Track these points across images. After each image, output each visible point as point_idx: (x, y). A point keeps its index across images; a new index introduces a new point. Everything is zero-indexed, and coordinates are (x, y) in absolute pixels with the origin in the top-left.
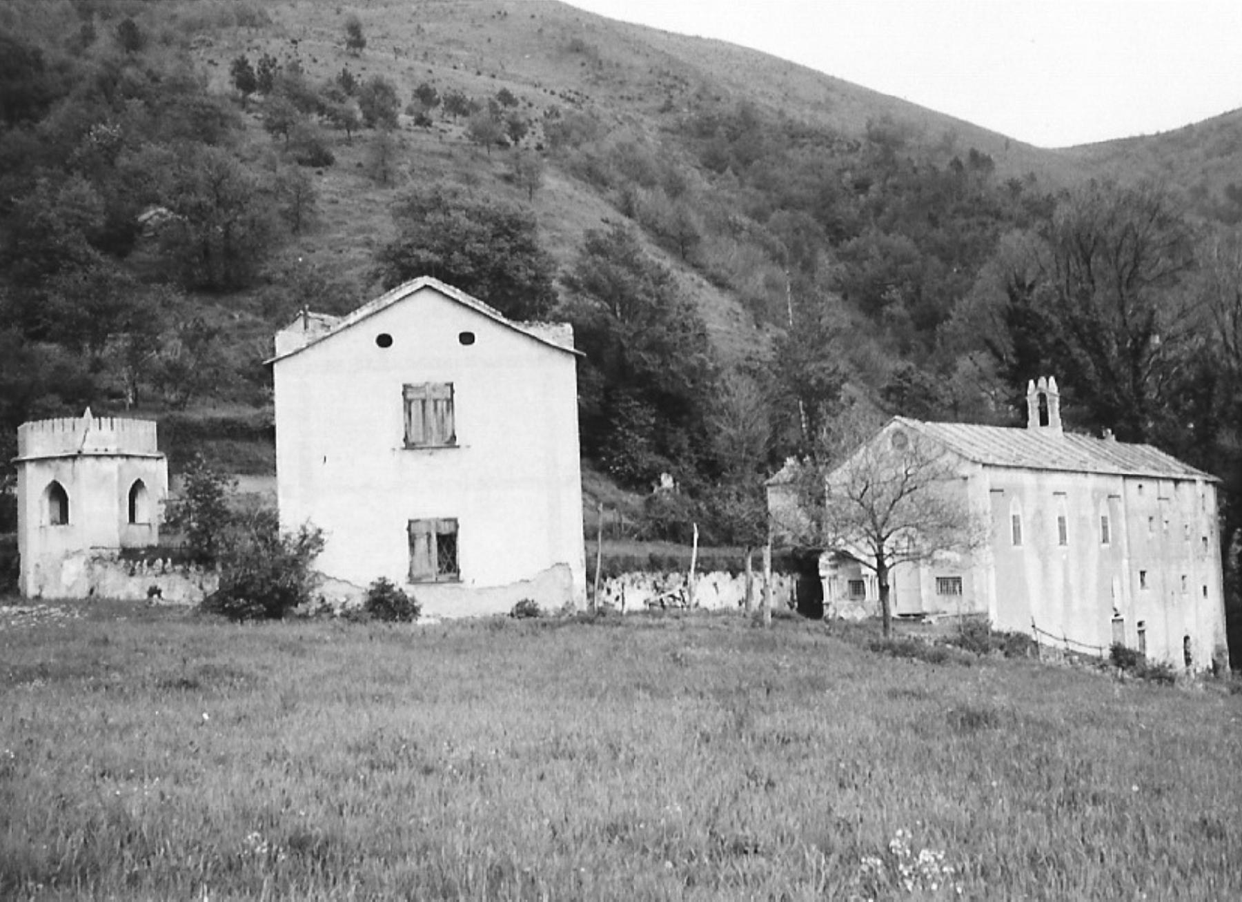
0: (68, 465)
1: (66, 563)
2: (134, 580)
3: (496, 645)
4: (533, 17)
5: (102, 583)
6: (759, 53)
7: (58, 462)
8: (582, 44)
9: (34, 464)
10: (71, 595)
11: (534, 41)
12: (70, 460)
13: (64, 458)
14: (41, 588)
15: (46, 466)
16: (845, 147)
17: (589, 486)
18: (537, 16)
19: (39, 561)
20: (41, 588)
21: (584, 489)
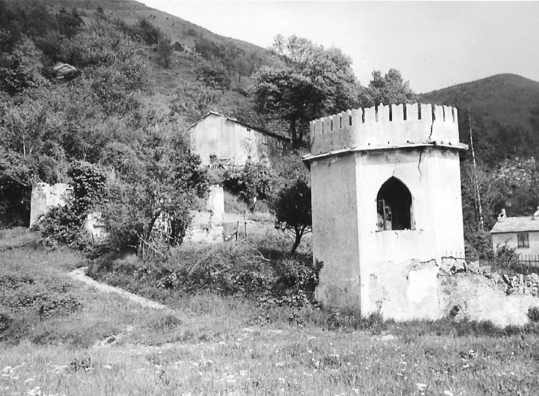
0: (412, 160)
1: (412, 274)
2: (511, 298)
3: (139, 336)
4: (168, 19)
5: (471, 302)
6: (259, 47)
7: (397, 154)
8: (194, 31)
9: (365, 157)
10: (421, 315)
11: (171, 29)
12: (415, 153)
13: (407, 150)
14: (379, 303)
15: (383, 159)
16: (204, 103)
17: (469, 235)
18: (169, 19)
19: (375, 271)
20: (379, 303)
21: (466, 238)
